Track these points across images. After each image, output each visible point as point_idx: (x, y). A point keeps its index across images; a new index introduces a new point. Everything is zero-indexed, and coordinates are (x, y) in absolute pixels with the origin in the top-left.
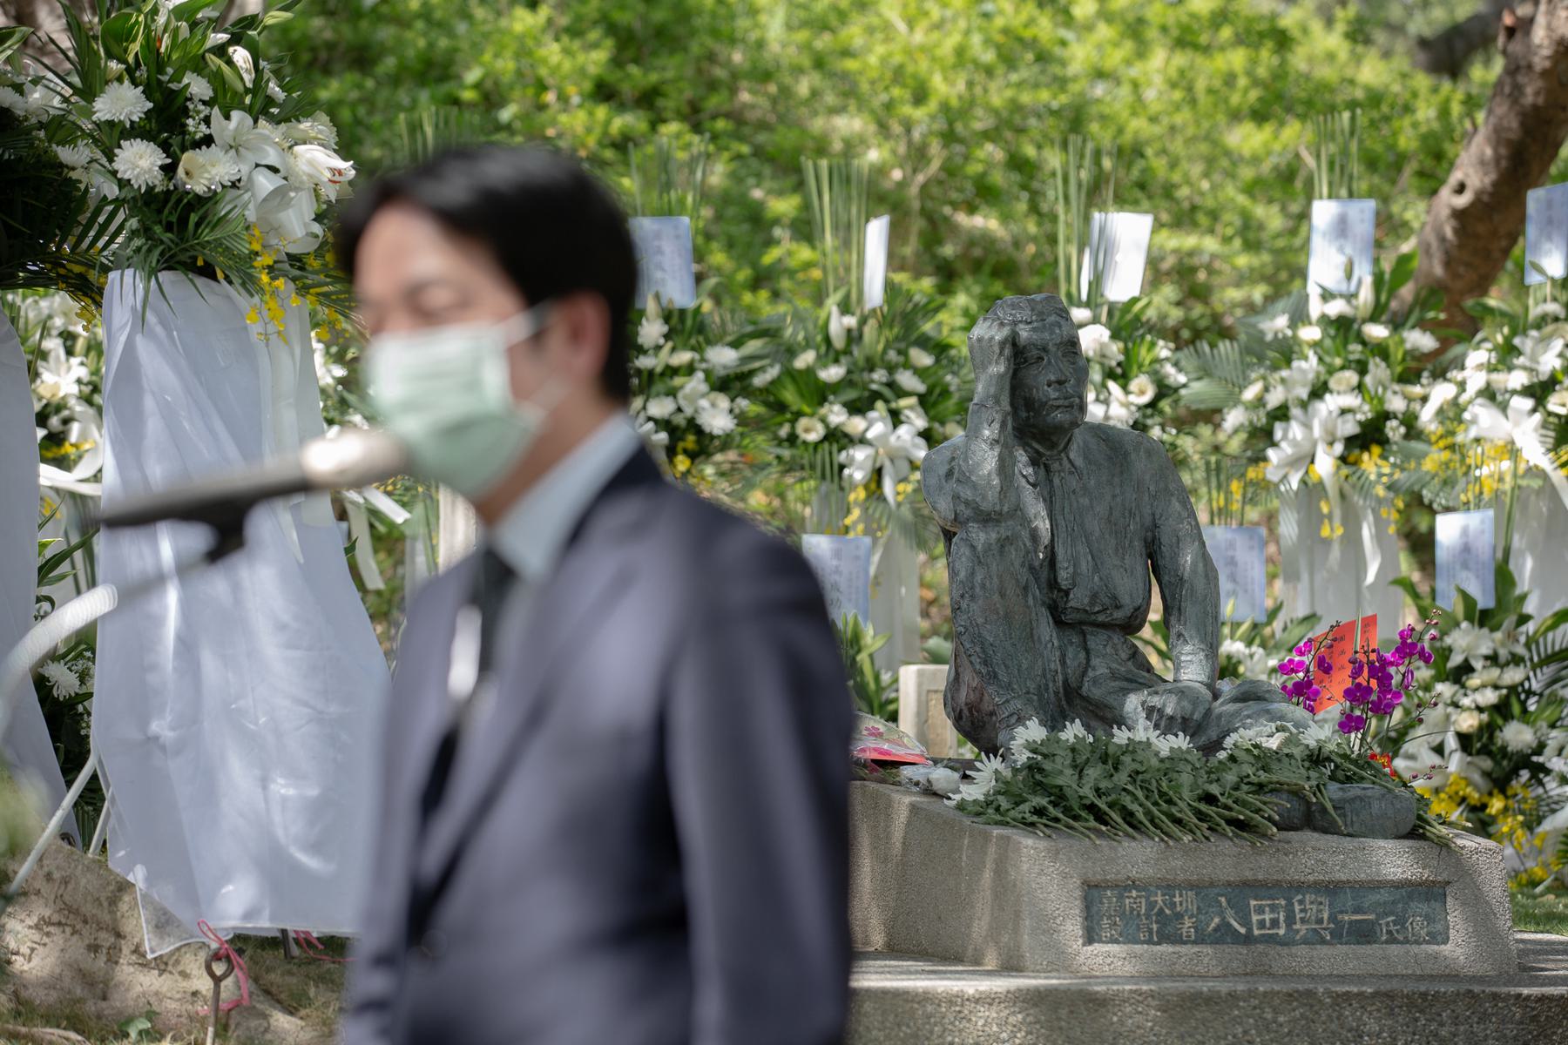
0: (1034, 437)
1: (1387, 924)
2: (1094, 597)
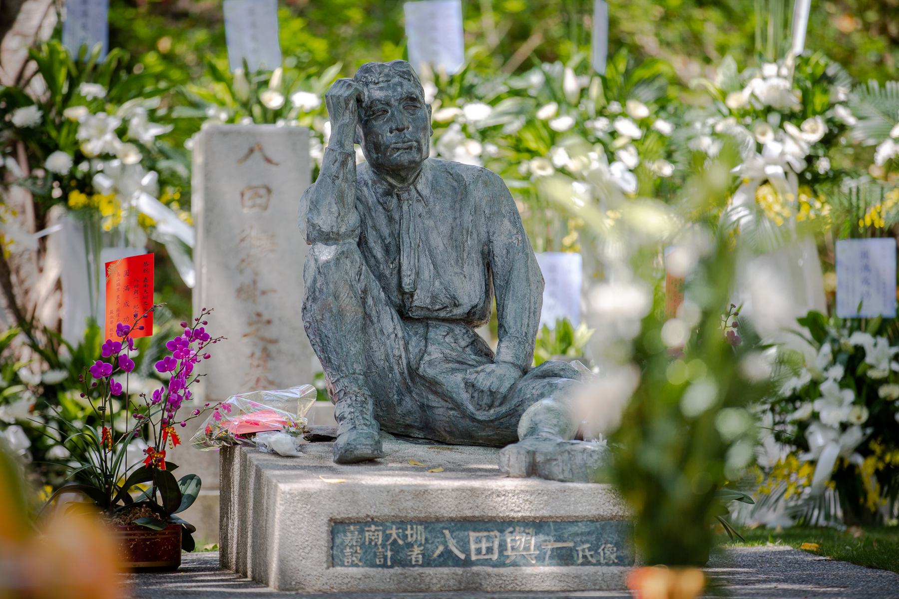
0: (388, 174)
1: (583, 550)
2: (434, 298)
